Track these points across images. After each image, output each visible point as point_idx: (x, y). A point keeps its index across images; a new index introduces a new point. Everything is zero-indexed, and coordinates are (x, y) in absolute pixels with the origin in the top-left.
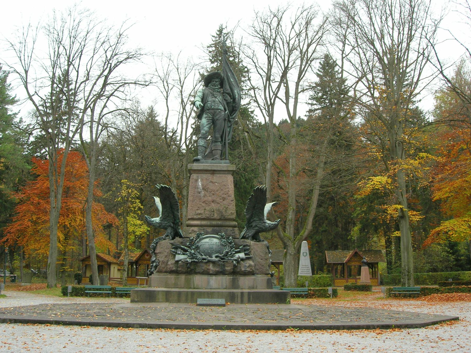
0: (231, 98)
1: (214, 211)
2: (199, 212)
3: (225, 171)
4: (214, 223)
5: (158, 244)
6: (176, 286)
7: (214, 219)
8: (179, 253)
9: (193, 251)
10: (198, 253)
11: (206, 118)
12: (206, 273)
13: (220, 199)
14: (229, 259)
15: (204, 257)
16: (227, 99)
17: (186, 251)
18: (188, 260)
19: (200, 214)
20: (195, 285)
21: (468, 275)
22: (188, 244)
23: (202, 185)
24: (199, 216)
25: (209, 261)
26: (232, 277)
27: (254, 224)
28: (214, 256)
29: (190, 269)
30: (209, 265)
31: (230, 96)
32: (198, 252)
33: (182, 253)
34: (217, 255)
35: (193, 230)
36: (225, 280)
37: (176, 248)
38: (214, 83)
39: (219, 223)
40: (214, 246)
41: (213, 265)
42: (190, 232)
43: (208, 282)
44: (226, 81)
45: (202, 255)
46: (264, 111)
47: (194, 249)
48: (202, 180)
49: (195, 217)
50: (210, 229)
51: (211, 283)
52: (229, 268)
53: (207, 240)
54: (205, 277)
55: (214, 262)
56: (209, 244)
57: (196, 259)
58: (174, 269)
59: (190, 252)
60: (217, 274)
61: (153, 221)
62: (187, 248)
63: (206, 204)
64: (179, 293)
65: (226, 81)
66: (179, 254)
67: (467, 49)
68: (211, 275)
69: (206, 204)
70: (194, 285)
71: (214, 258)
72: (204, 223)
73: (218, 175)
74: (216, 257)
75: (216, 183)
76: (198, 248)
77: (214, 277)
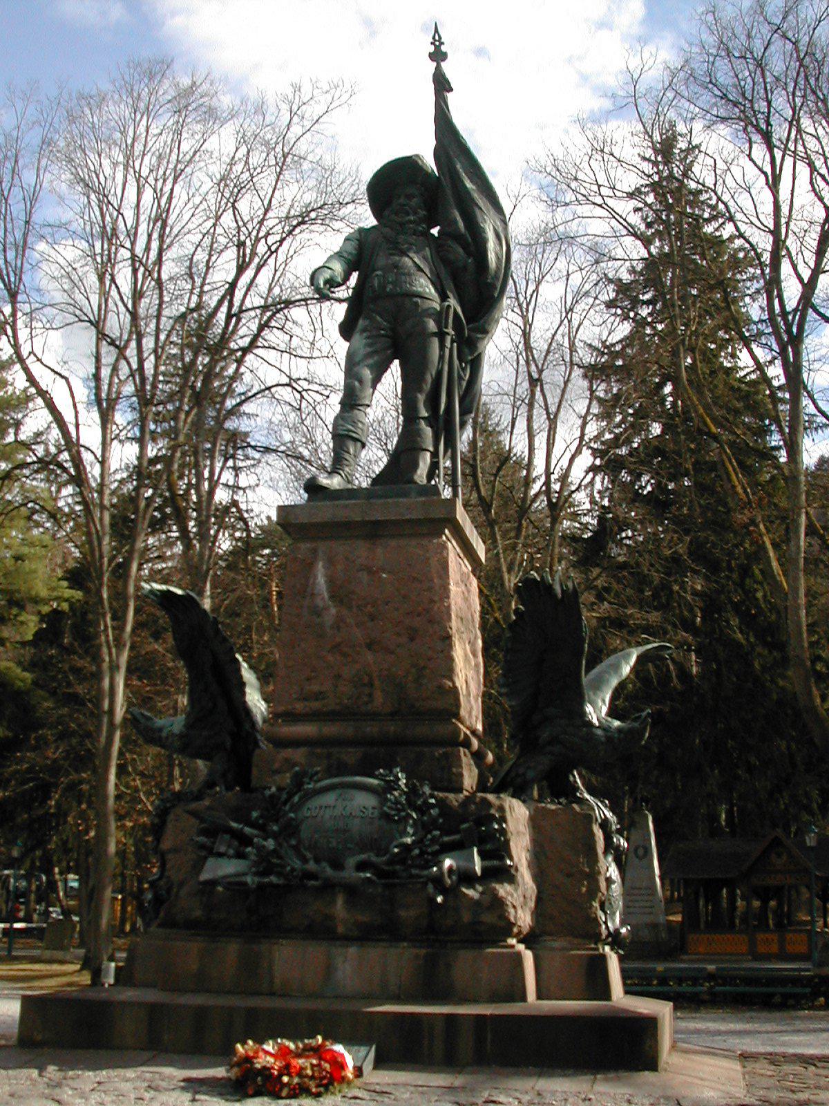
0: (469, 254)
1: (371, 685)
2: (315, 688)
3: (418, 522)
4: (371, 729)
5: (171, 817)
6: (201, 983)
7: (373, 716)
8: (222, 849)
9: (270, 844)
10: (291, 852)
11: (364, 331)
12: (322, 931)
13: (399, 634)
14: (411, 876)
15: (312, 866)
16: (452, 257)
17: (246, 841)
18: (249, 879)
19: (318, 696)
20: (277, 981)
21: (3, 1042)
22: (255, 814)
23: (331, 581)
24: (316, 705)
25: (329, 887)
26: (423, 952)
27: (545, 735)
28: (351, 862)
29: (261, 912)
30: (333, 902)
31: (465, 247)
32: (296, 848)
33: (231, 852)
34: (363, 857)
35: (287, 760)
36: (399, 959)
37: (212, 832)
38: (402, 200)
39: (392, 728)
40: (355, 825)
41: (347, 902)
42: (276, 766)
43: (329, 969)
44: (449, 192)
45: (305, 860)
46: (117, 297)
47: (275, 836)
48: (330, 562)
49: (299, 707)
50: (351, 756)
51: (340, 974)
52: (412, 913)
53: (329, 798)
54: (315, 952)
55: (352, 891)
56: (337, 812)
57: (279, 875)
58: (198, 913)
59: (260, 848)
60: (364, 936)
61: (161, 730)
62: (255, 832)
63: (345, 655)
64: (201, 1014)
65: (449, 192)
66: (220, 855)
67: (438, 55)
68: (347, 939)
69: (345, 655)
70: (271, 982)
71: (350, 874)
72: (331, 729)
73: (393, 543)
74: (361, 866)
75: (384, 571)
76: (291, 829)
77: (353, 950)
